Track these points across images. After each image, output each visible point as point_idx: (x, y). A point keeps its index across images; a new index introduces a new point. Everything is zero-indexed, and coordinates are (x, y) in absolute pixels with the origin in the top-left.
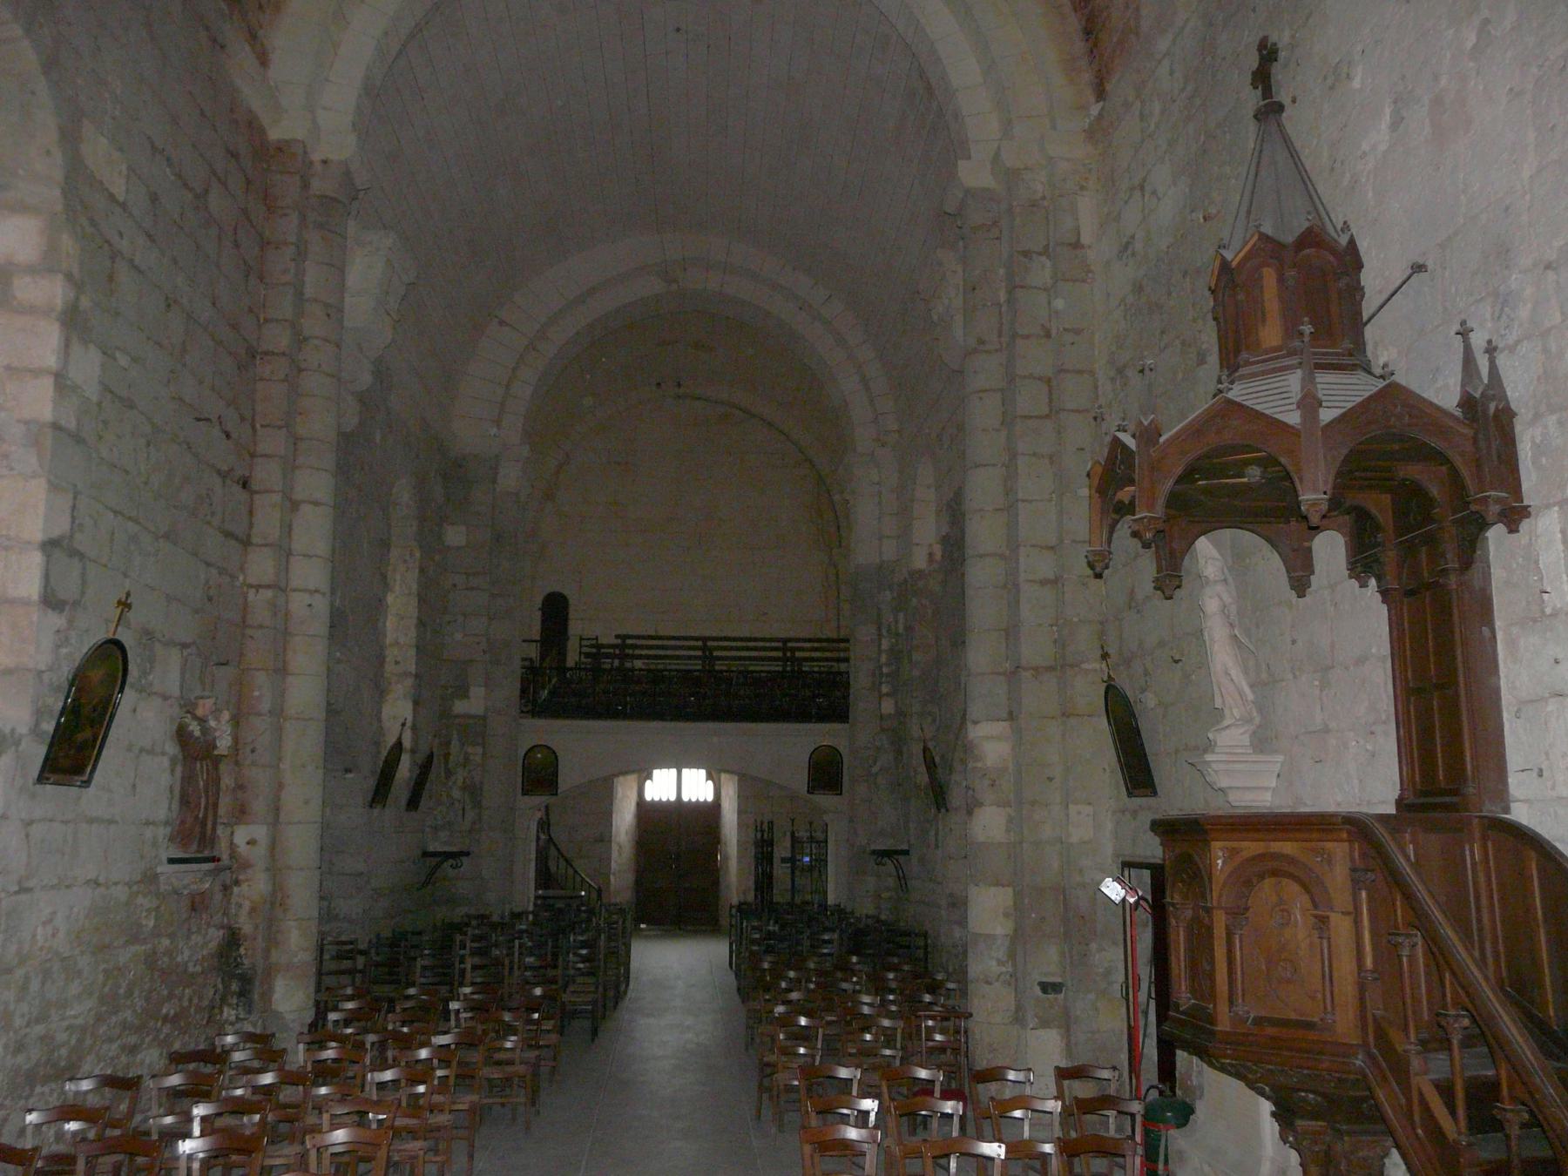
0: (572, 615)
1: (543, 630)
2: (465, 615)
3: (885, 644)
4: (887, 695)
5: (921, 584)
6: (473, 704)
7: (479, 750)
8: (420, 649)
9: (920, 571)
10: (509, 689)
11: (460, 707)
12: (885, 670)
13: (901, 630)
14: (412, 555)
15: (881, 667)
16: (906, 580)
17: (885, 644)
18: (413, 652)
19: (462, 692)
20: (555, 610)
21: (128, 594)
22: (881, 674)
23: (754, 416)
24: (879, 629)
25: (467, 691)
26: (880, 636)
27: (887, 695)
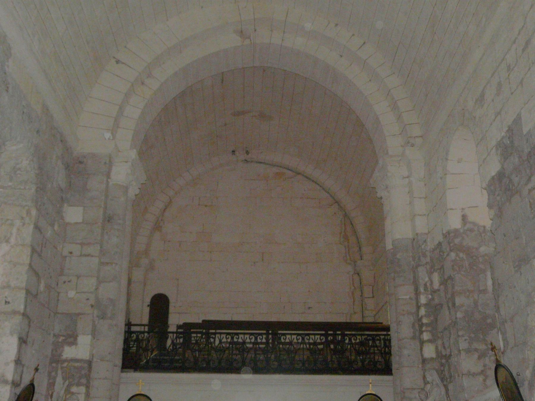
0: (171, 309)
1: (151, 317)
2: (78, 277)
3: (423, 300)
4: (429, 341)
5: (457, 241)
6: (80, 350)
7: (83, 389)
8: (31, 294)
9: (456, 231)
10: (113, 343)
11: (69, 352)
12: (425, 321)
13: (436, 285)
14: (28, 212)
15: (420, 320)
16: (440, 244)
17: (423, 300)
18: (22, 295)
19: (71, 339)
20: (160, 305)
21: (38, 365)
22: (422, 325)
23: (299, 174)
24: (416, 289)
25: (76, 339)
26: (417, 293)
27: (429, 341)
